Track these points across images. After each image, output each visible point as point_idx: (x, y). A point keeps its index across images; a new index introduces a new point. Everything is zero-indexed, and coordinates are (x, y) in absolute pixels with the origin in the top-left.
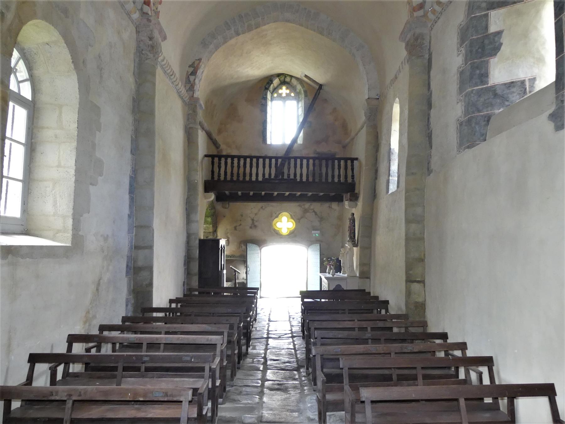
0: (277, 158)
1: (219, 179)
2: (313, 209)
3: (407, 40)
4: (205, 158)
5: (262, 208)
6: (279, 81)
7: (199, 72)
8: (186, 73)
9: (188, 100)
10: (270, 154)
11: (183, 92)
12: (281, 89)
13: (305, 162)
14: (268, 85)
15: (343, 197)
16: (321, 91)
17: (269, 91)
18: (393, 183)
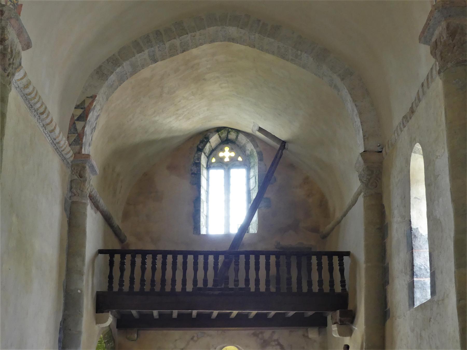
0: (216, 254)
1: (120, 290)
2: (277, 340)
3: (433, 40)
4: (99, 254)
5: (192, 339)
6: (219, 139)
7: (92, 116)
8: (70, 118)
9: (72, 159)
10: (206, 249)
11: (62, 143)
12: (223, 150)
13: (262, 259)
14: (202, 145)
15: (326, 318)
16: (284, 151)
17: (203, 153)
18: (420, 288)
